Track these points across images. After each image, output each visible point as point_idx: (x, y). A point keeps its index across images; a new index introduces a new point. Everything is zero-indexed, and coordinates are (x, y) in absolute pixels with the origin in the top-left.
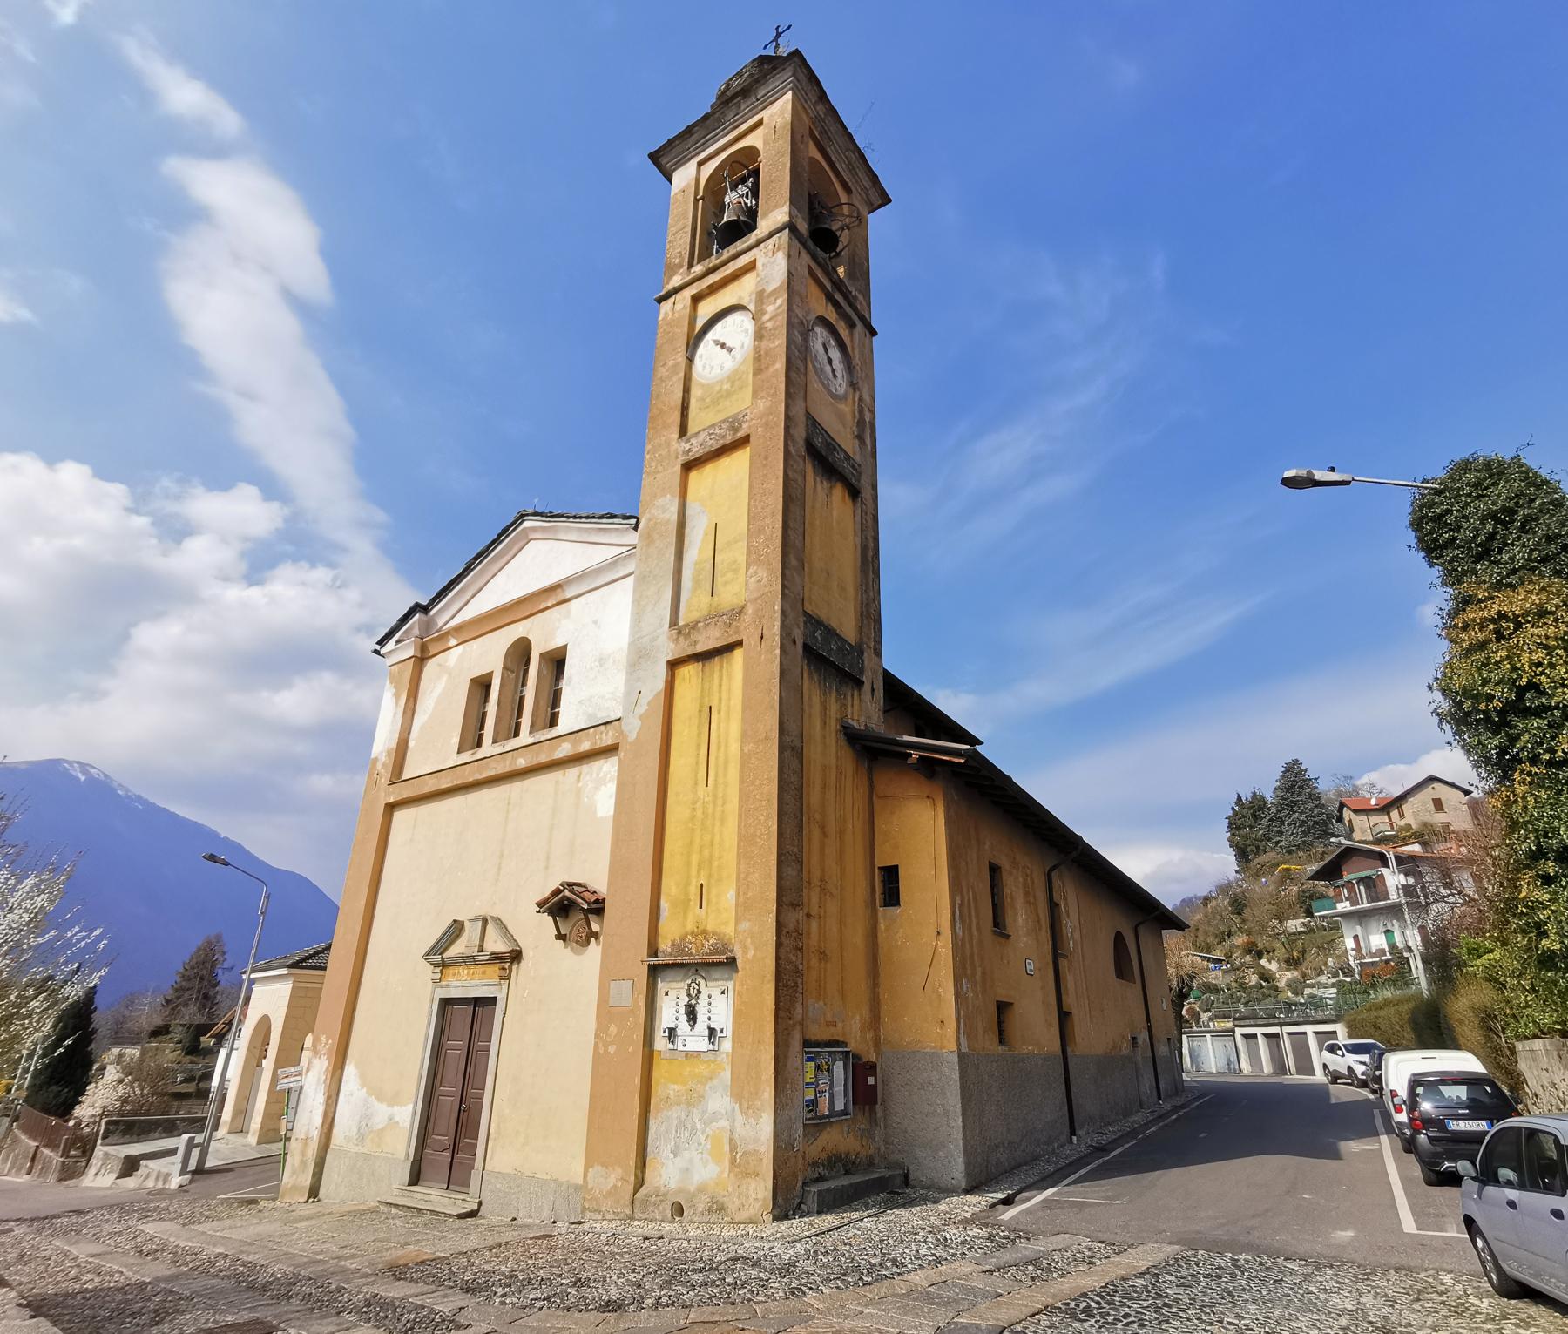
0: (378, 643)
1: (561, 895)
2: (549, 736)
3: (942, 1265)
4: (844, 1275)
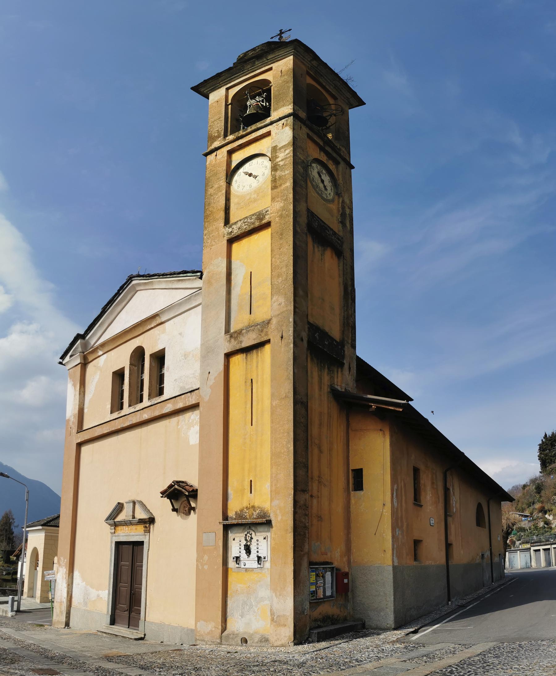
0: (61, 358)
1: (174, 488)
2: (159, 401)
3: (381, 660)
4: (331, 666)
